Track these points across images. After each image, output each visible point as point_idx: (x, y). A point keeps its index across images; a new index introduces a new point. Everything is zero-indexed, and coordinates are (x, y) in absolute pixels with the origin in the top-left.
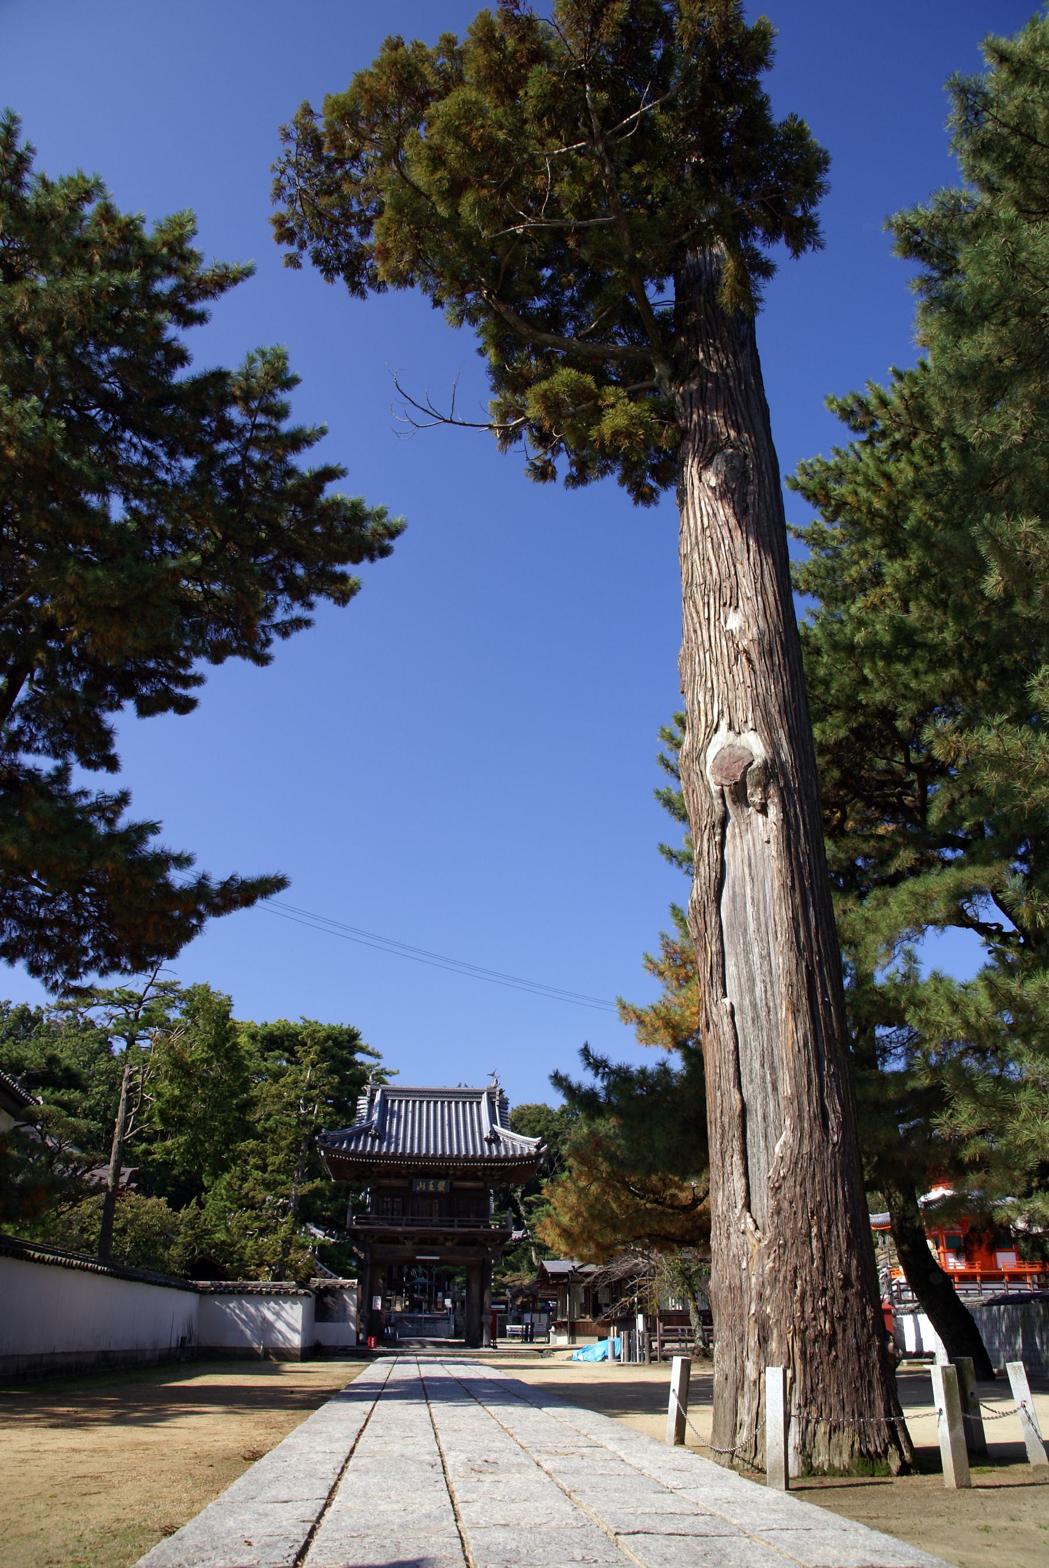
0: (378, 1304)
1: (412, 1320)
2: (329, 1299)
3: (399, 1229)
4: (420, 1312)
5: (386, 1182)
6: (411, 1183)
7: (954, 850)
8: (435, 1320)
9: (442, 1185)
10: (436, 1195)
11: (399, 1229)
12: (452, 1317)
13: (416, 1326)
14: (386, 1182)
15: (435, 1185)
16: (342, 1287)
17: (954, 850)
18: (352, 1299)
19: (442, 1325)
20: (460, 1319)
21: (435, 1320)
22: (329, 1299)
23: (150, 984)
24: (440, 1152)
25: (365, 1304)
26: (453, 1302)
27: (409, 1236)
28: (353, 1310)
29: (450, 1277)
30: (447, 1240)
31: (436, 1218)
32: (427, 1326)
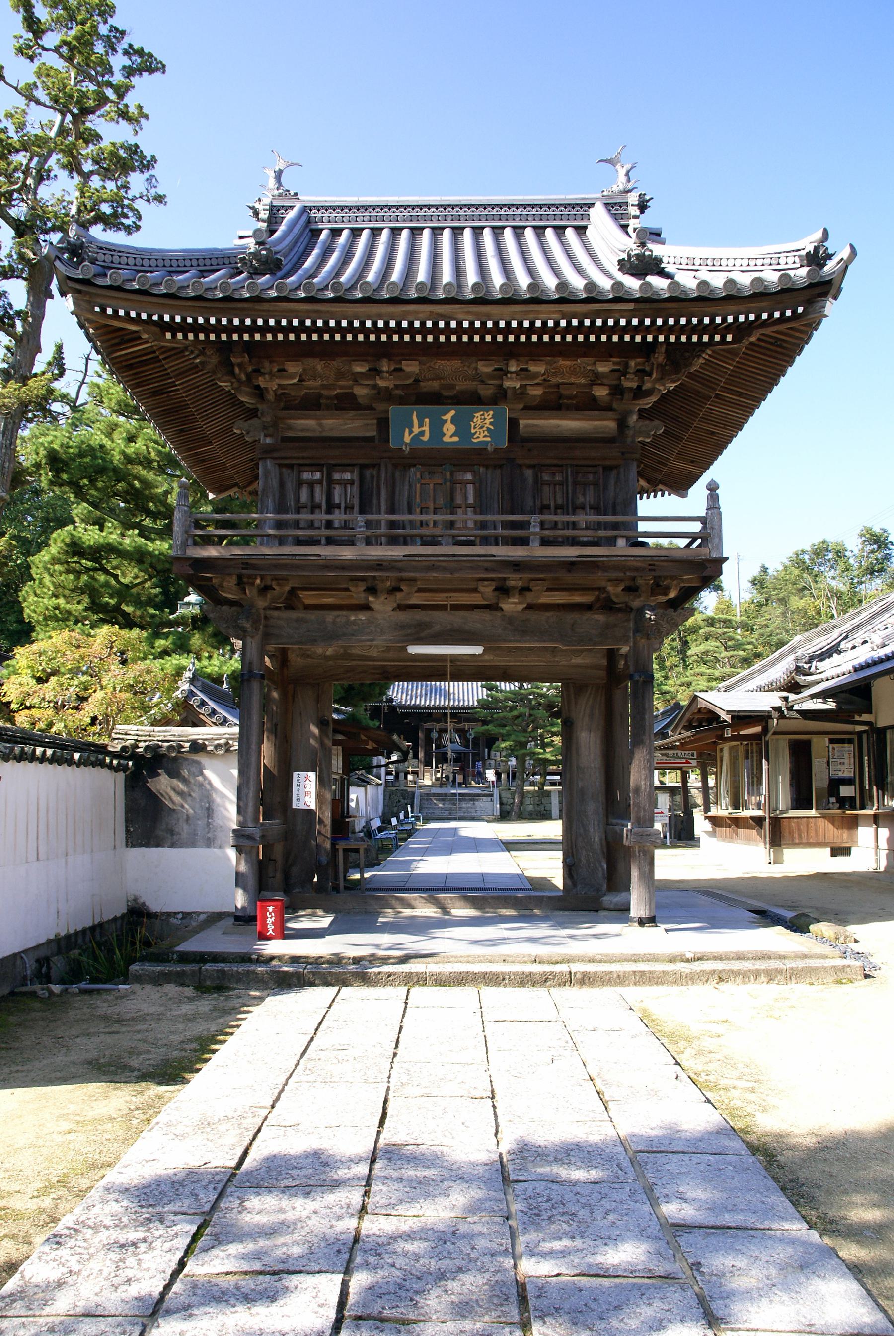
0: (306, 791)
1: (443, 798)
2: (163, 784)
3: (347, 553)
4: (453, 786)
5: (306, 424)
6: (383, 424)
7: (273, 923)
8: (473, 798)
9: (483, 426)
10: (467, 458)
11: (347, 553)
12: (496, 792)
13: (448, 805)
14: (306, 424)
15: (463, 428)
16: (197, 747)
17: (273, 923)
18: (224, 778)
19: (482, 804)
20: (506, 795)
21: (473, 798)
22: (163, 784)
23: (83, 383)
24: (472, 277)
25: (267, 794)
26: (498, 774)
27: (374, 580)
28: (229, 813)
29: (491, 741)
30: (503, 590)
31: (467, 519)
32: (464, 805)
